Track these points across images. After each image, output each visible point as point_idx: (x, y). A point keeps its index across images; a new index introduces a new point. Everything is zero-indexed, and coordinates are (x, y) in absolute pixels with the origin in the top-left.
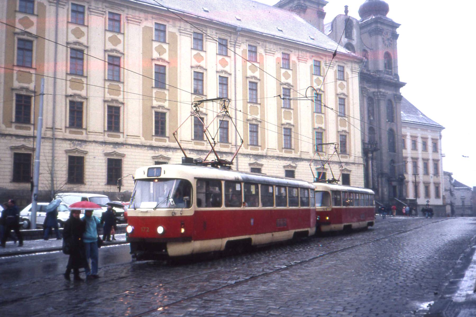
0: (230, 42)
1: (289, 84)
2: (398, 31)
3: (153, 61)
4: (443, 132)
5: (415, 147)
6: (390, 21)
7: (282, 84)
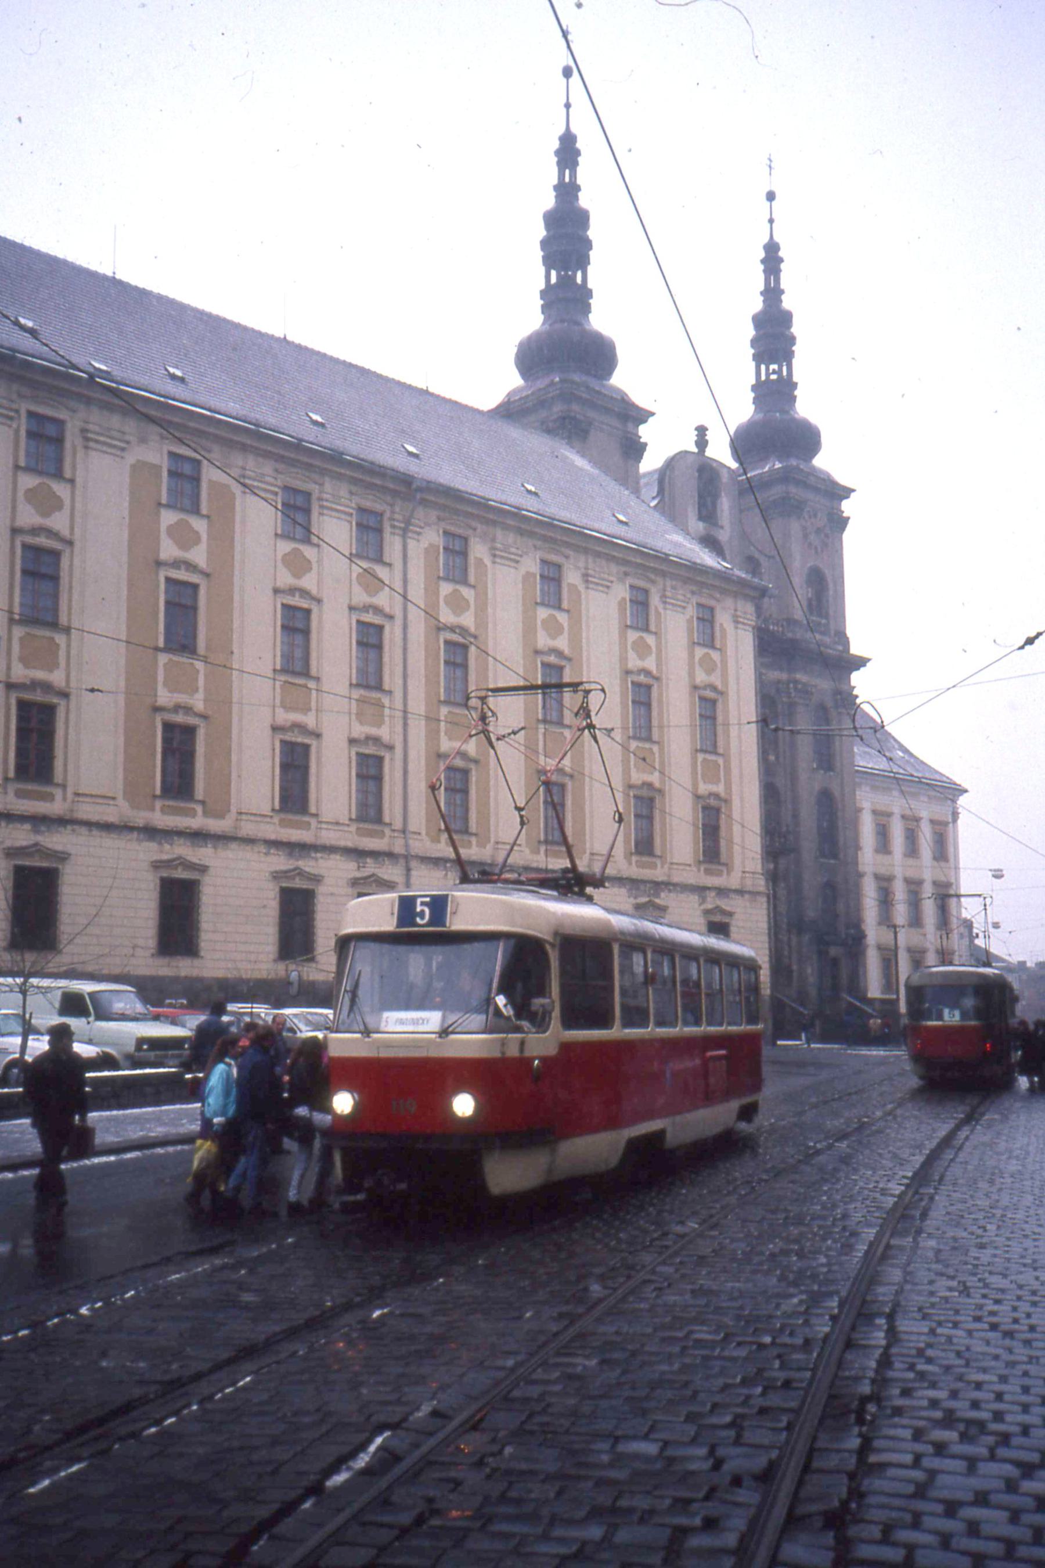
0: (392, 519)
1: (463, 631)
2: (847, 507)
3: (278, 595)
4: (962, 801)
5: (884, 845)
6: (824, 480)
7: (439, 629)
